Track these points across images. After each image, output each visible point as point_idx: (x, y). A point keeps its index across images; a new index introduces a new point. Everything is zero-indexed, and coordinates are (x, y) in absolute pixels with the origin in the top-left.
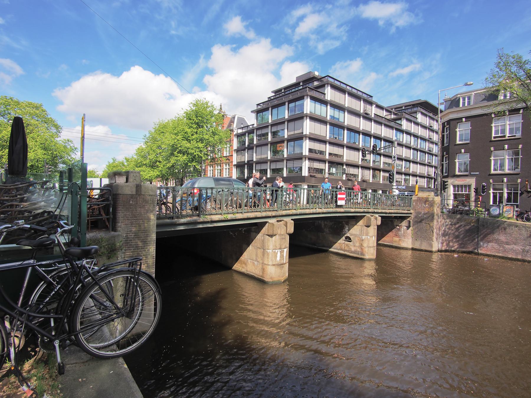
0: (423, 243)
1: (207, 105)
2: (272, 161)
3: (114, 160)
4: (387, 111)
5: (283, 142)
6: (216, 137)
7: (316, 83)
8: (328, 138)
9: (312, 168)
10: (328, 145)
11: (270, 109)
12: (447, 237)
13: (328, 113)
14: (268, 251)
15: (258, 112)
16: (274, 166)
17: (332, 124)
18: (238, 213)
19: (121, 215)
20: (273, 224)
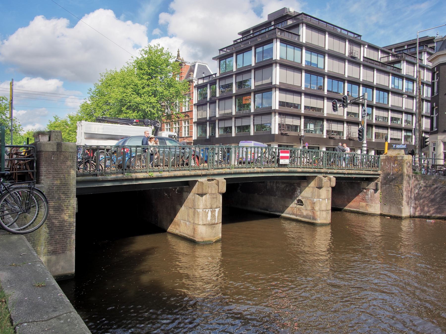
0: (392, 207)
1: (162, 52)
2: (237, 118)
3: (56, 118)
4: (383, 52)
5: (249, 94)
6: (172, 90)
7: (290, 22)
8: (303, 89)
9: (283, 125)
10: (303, 97)
11: (234, 55)
12: (421, 201)
13: (305, 58)
14: (199, 210)
15: (221, 58)
16: (240, 123)
17: (307, 71)
18: (164, 171)
19: (43, 169)
20: (202, 183)
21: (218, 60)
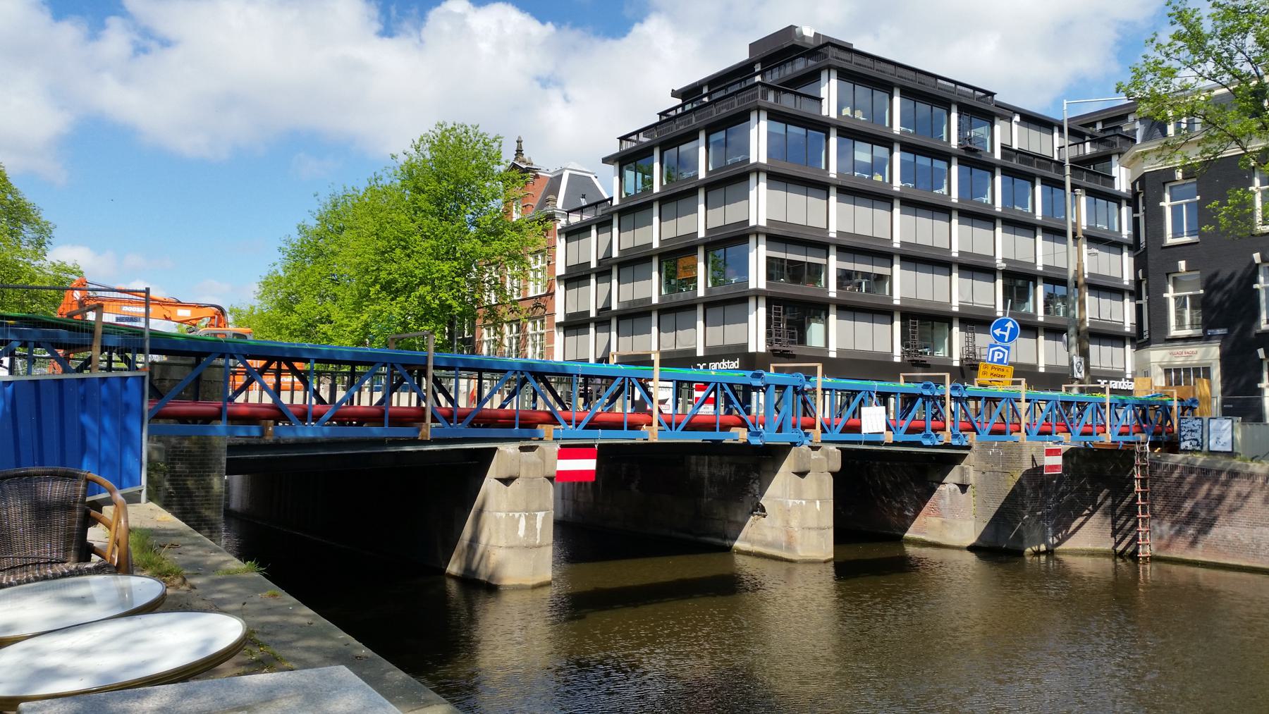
7: (800, 66)
21: (617, 165)
